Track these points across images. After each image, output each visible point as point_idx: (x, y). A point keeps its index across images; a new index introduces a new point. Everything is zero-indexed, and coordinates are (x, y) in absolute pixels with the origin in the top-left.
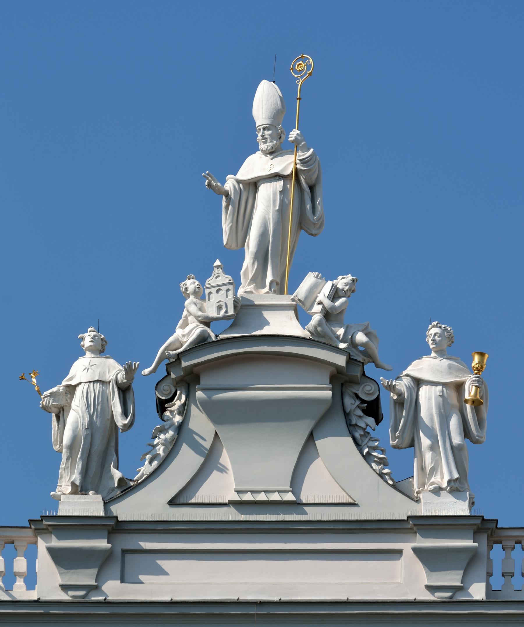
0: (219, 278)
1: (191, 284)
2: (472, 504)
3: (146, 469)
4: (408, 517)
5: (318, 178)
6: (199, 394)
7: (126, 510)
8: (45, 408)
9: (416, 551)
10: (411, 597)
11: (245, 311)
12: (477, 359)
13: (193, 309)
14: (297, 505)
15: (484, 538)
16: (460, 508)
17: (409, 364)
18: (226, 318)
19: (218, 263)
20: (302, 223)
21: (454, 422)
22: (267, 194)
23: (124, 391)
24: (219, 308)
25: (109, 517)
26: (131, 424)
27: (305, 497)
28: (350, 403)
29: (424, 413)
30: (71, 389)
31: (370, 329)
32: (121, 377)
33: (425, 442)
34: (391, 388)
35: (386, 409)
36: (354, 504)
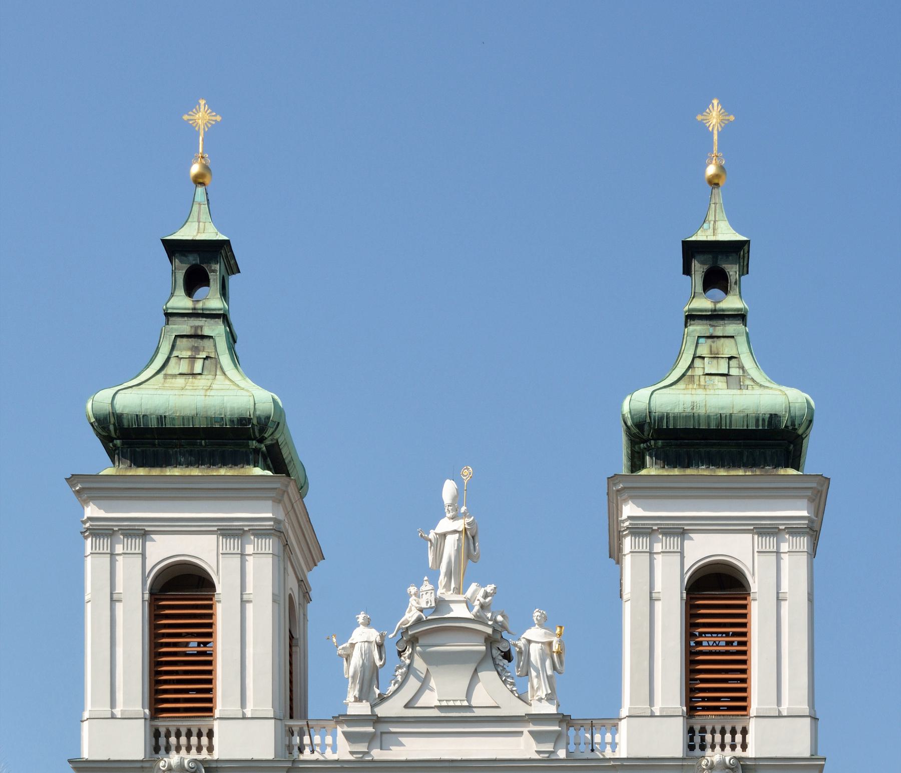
0: (427, 586)
1: (412, 589)
2: (558, 706)
3: (392, 688)
4: (617, 744)
5: (476, 533)
6: (418, 648)
7: (383, 711)
8: (340, 655)
9: (530, 732)
10: (528, 757)
11: (441, 604)
12: (558, 629)
13: (414, 603)
14: (470, 707)
15: (564, 725)
16: (551, 709)
17: (524, 632)
18: (431, 608)
19: (426, 578)
20: (469, 556)
21: (548, 663)
22: (451, 544)
23: (380, 646)
24: (427, 602)
25: (374, 715)
26: (384, 664)
27: (473, 704)
28: (496, 653)
29: (532, 659)
30: (353, 645)
31: (505, 613)
32: (378, 639)
33: (534, 674)
34: (515, 645)
35: (514, 653)
36: (498, 707)
